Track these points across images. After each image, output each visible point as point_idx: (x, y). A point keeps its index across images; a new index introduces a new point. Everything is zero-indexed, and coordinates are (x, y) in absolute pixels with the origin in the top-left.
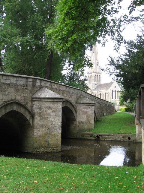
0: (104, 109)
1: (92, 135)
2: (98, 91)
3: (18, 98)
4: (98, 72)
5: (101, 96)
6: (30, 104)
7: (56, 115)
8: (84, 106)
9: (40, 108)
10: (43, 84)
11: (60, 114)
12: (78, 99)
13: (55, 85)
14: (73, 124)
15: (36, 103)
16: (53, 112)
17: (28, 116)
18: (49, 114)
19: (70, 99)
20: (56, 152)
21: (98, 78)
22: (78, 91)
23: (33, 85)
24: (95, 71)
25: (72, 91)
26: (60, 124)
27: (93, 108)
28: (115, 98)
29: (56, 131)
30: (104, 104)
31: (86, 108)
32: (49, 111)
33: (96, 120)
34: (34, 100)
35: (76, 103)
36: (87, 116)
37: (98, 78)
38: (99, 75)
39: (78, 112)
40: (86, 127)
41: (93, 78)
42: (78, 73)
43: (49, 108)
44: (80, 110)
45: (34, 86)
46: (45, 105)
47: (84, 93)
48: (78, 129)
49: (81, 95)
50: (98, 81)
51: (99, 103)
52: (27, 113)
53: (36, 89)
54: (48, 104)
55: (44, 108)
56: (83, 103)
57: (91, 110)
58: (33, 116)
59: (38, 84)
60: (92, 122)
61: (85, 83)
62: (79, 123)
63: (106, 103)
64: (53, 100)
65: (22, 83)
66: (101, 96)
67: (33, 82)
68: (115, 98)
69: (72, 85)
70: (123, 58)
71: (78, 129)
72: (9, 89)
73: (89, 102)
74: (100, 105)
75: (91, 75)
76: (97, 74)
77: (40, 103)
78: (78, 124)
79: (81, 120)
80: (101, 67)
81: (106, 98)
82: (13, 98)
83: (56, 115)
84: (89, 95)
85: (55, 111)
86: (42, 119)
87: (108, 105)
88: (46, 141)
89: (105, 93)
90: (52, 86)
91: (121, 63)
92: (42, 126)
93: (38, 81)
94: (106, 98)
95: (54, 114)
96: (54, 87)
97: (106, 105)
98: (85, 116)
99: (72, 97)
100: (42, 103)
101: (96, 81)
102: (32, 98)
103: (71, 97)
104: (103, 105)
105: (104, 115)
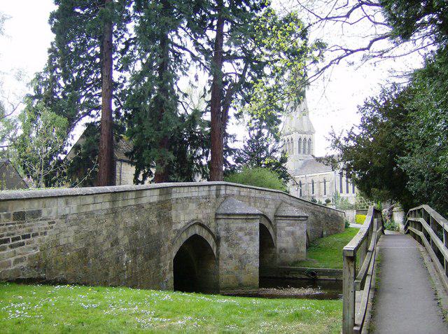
0: (323, 222)
1: (301, 272)
2: (307, 176)
3: (200, 216)
4: (306, 130)
5: (313, 186)
6: (213, 224)
7: (252, 239)
8: (288, 221)
9: (228, 230)
10: (228, 192)
11: (257, 238)
12: (277, 209)
13: (245, 190)
14: (270, 252)
15: (222, 222)
16: (246, 235)
17: (211, 242)
18: (240, 239)
19: (266, 210)
20: (270, 278)
21: (307, 145)
22: (277, 194)
23: (216, 195)
24: (299, 129)
25: (268, 196)
26: (257, 252)
27: (304, 224)
28: (348, 192)
29: (251, 265)
30: (322, 213)
31: (292, 225)
32: (241, 234)
33: (310, 245)
34: (220, 217)
35: (275, 216)
36: (295, 239)
37: (307, 145)
38: (308, 137)
39: (278, 232)
40: (292, 257)
41: (296, 144)
42: (268, 146)
43: (241, 229)
44: (282, 228)
45: (218, 196)
46: (235, 225)
47: (287, 197)
48: (278, 261)
49: (283, 201)
50: (307, 151)
51: (313, 213)
52: (211, 236)
53: (221, 200)
54: (239, 224)
55: (234, 229)
56: (287, 217)
57: (301, 228)
58: (218, 240)
59: (223, 192)
60: (304, 249)
61: (224, 75)
62: (281, 251)
63: (326, 212)
64: (248, 217)
65: (204, 194)
66: (313, 186)
67: (217, 190)
68: (348, 192)
69: (270, 187)
70: (357, 132)
71: (278, 261)
72: (191, 204)
73: (297, 214)
74: (316, 216)
75: (289, 137)
76: (303, 136)
77: (226, 221)
78: (278, 252)
79: (284, 245)
80: (316, 156)
81: (325, 190)
82: (195, 218)
83: (252, 239)
84: (295, 199)
85: (250, 234)
86: (230, 246)
87: (330, 215)
88: (237, 279)
89: (322, 180)
90: (240, 192)
91: (352, 143)
92: (231, 257)
93: (223, 188)
94: (325, 190)
95: (248, 237)
96: (242, 194)
97: (327, 216)
98: (290, 239)
99: (269, 207)
100: (231, 221)
101: (302, 150)
102: (216, 214)
103: (267, 207)
104: (322, 216)
105: (322, 236)
